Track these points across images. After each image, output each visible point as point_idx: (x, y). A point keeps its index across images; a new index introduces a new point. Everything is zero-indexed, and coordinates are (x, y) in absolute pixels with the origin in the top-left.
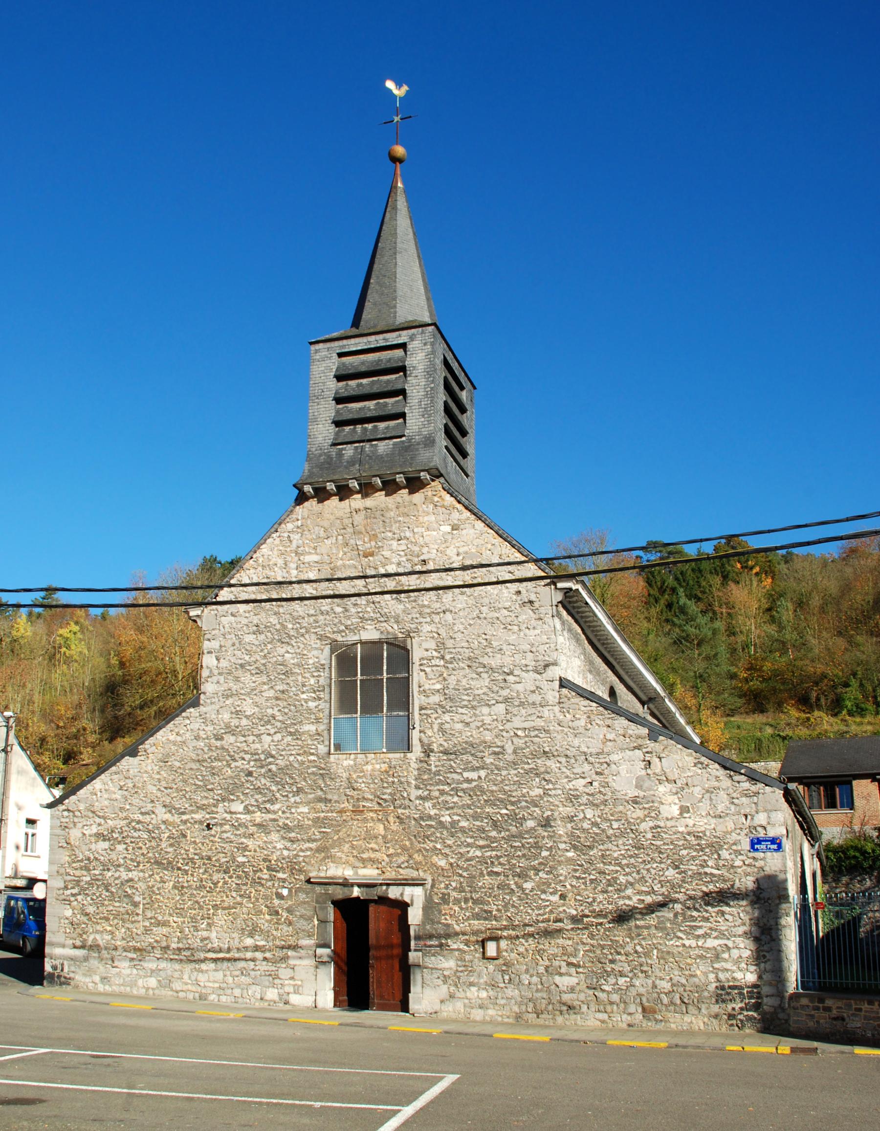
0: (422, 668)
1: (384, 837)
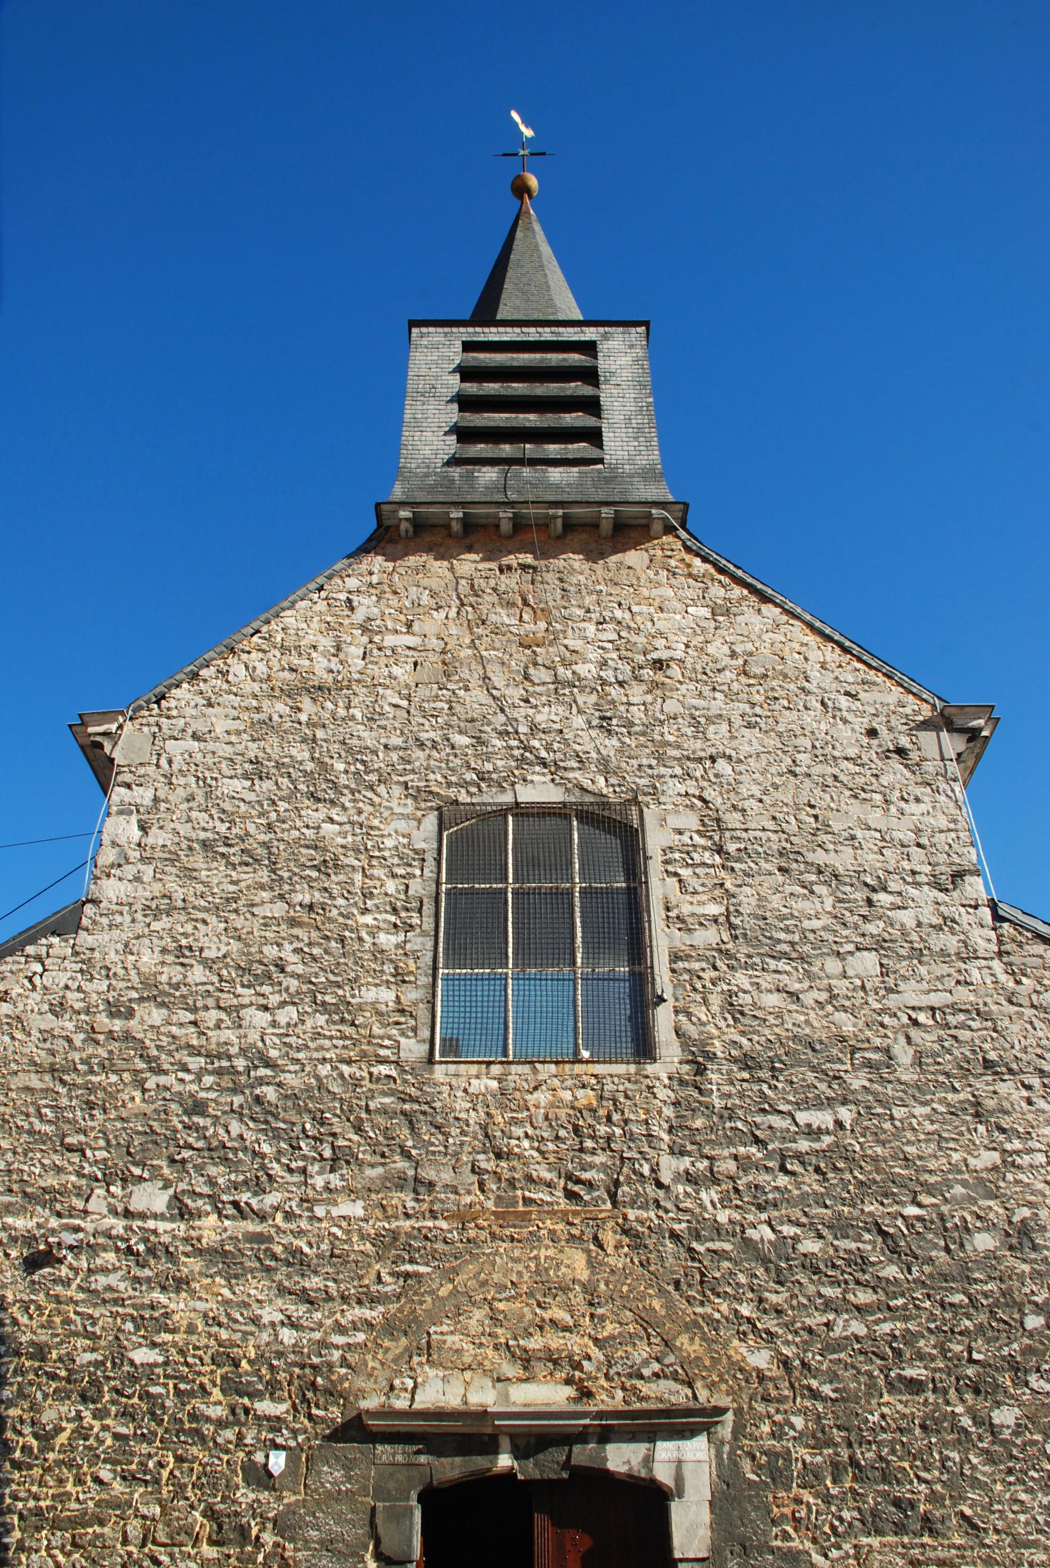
0: (670, 868)
1: (589, 1289)
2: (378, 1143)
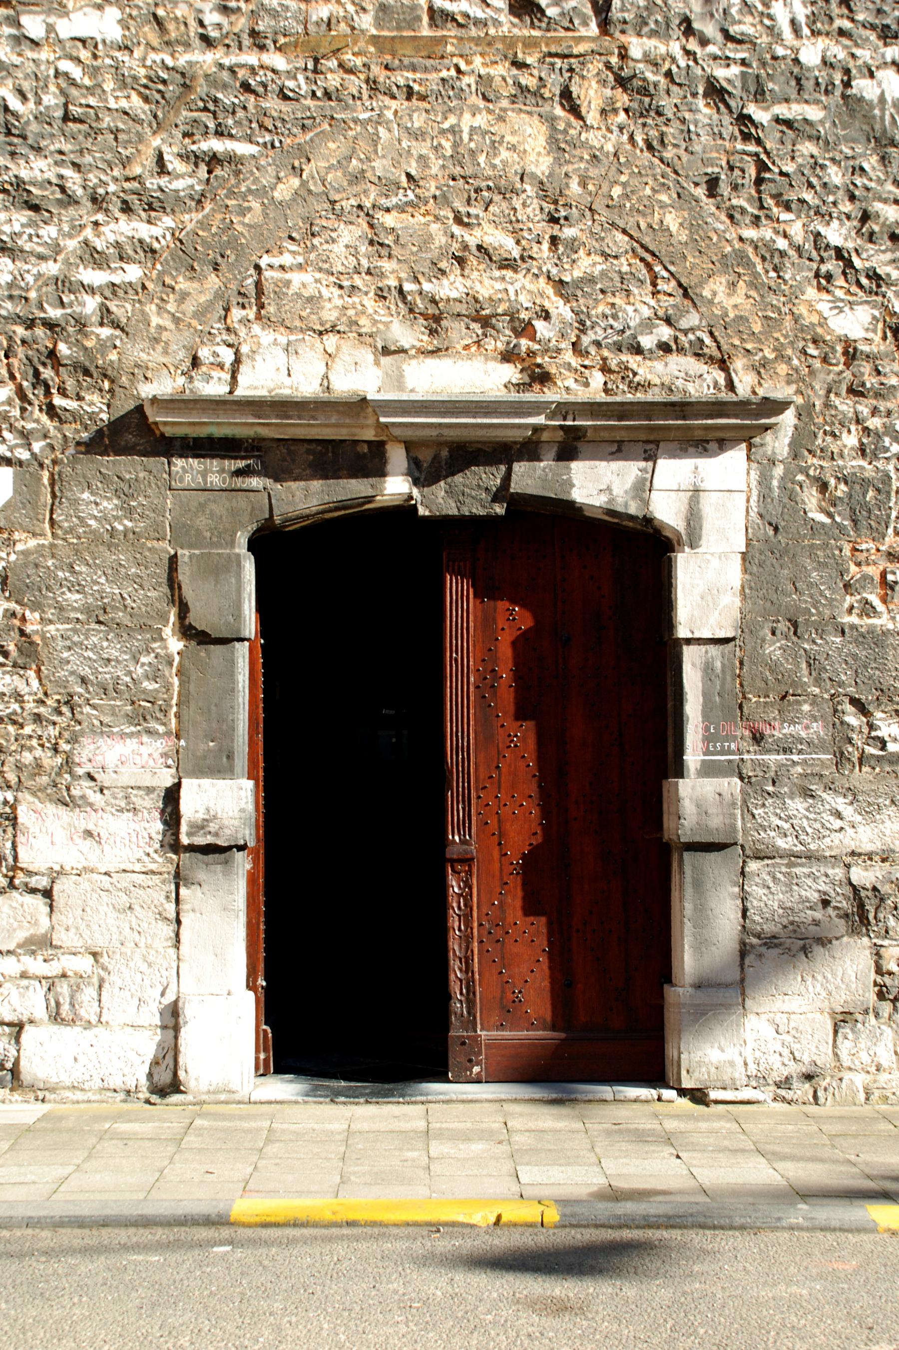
1: (551, 195)
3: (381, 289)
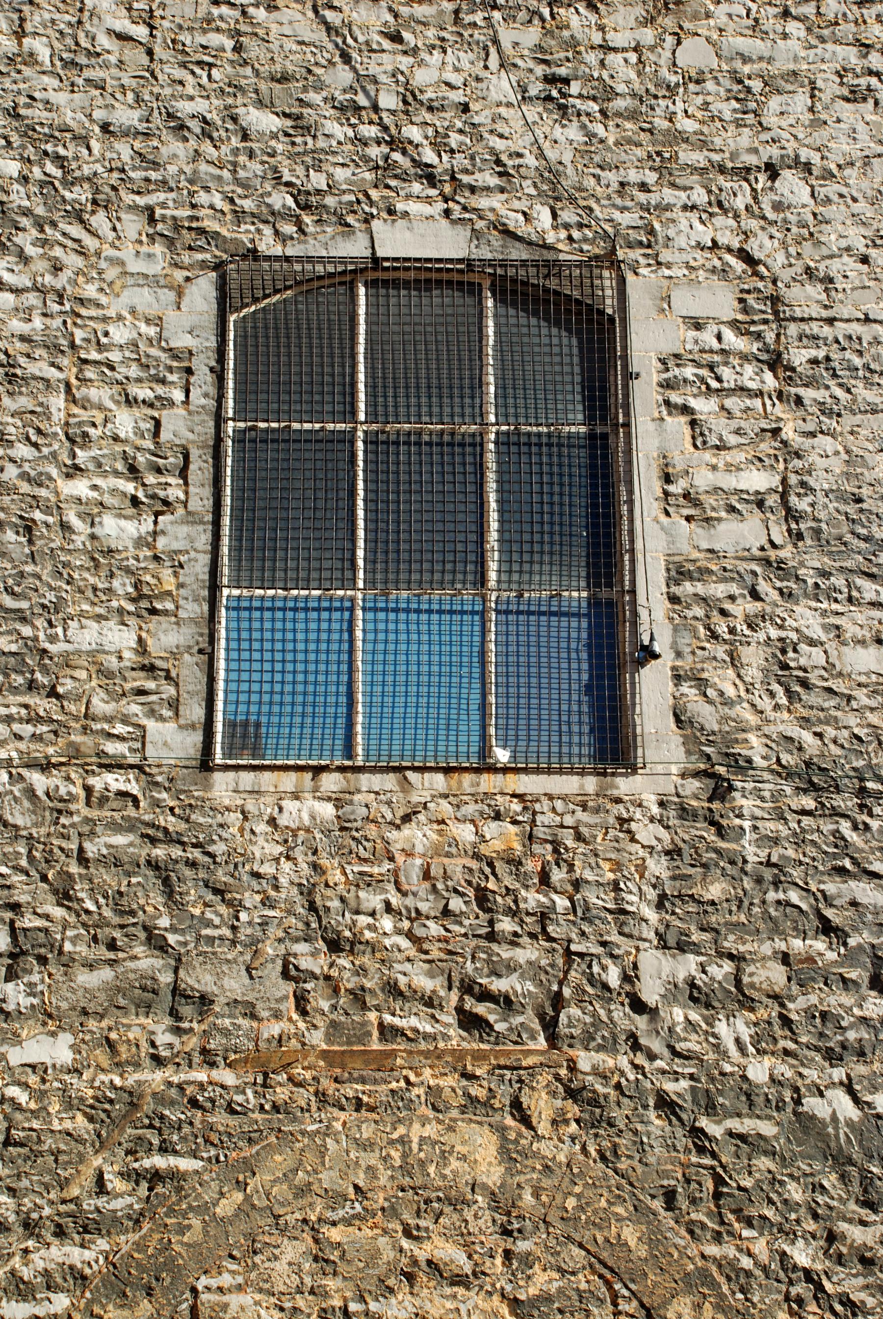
0: (676, 398)
1: (503, 1204)
2: (103, 923)
3: (324, 1310)
